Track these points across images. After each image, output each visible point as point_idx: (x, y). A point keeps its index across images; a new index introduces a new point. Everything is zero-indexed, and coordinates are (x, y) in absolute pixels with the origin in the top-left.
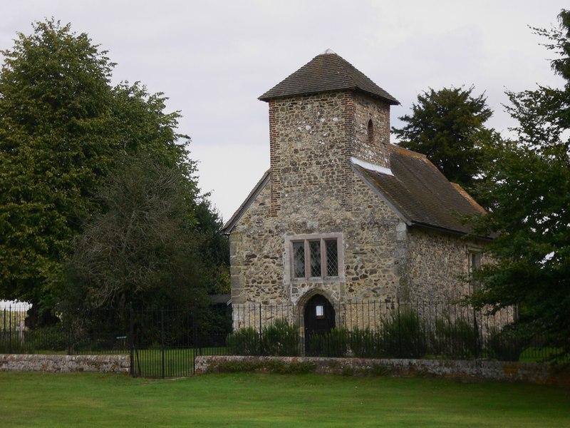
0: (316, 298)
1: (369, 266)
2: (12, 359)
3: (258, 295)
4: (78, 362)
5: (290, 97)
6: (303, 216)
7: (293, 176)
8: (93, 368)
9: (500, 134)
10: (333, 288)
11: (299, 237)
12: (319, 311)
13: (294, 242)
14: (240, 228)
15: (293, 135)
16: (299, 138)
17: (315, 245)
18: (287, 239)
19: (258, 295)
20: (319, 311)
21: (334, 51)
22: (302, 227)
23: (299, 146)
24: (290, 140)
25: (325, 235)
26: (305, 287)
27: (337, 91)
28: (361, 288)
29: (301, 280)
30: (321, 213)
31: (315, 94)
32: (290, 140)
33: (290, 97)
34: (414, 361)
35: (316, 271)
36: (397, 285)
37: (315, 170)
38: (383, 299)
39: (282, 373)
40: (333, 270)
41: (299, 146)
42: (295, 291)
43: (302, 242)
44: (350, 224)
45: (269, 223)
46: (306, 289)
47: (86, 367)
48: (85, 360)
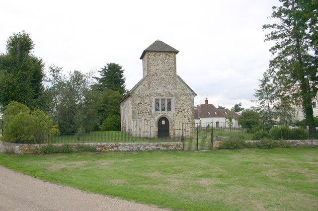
0: (163, 118)
1: (183, 108)
2: (120, 145)
3: (142, 116)
4: (157, 146)
5: (155, 51)
6: (160, 90)
7: (156, 77)
8: (165, 148)
9: (270, 61)
10: (170, 115)
11: (158, 98)
12: (163, 122)
13: (156, 99)
14: (136, 93)
15: (156, 64)
16: (158, 65)
17: (163, 100)
18: (154, 98)
19: (142, 116)
20: (163, 122)
21: (160, 40)
22: (159, 94)
23: (158, 68)
24: (155, 65)
25: (168, 98)
26: (160, 114)
27: (172, 52)
28: (180, 115)
29: (158, 112)
30: (166, 90)
31: (164, 52)
32: (155, 65)
33: (155, 51)
34: (293, 141)
35: (163, 109)
36: (192, 114)
37: (164, 76)
38: (187, 119)
39: (284, 147)
40: (169, 109)
41: (158, 68)
42: (156, 115)
43: (159, 100)
44: (176, 94)
45: (147, 92)
46: (161, 115)
47: (162, 148)
48: (160, 145)
